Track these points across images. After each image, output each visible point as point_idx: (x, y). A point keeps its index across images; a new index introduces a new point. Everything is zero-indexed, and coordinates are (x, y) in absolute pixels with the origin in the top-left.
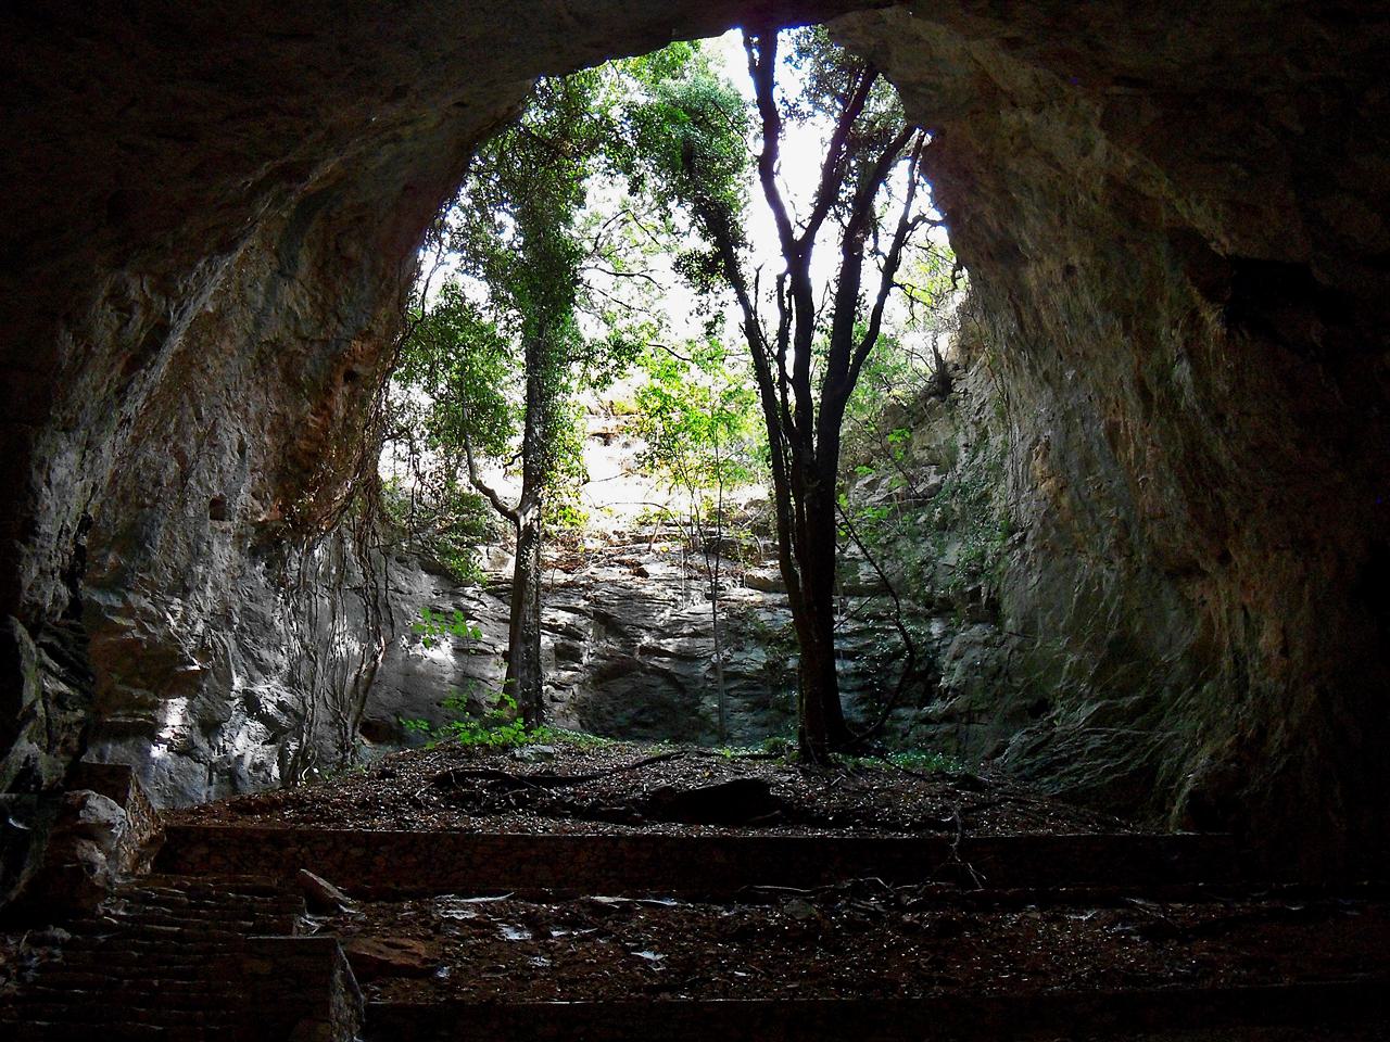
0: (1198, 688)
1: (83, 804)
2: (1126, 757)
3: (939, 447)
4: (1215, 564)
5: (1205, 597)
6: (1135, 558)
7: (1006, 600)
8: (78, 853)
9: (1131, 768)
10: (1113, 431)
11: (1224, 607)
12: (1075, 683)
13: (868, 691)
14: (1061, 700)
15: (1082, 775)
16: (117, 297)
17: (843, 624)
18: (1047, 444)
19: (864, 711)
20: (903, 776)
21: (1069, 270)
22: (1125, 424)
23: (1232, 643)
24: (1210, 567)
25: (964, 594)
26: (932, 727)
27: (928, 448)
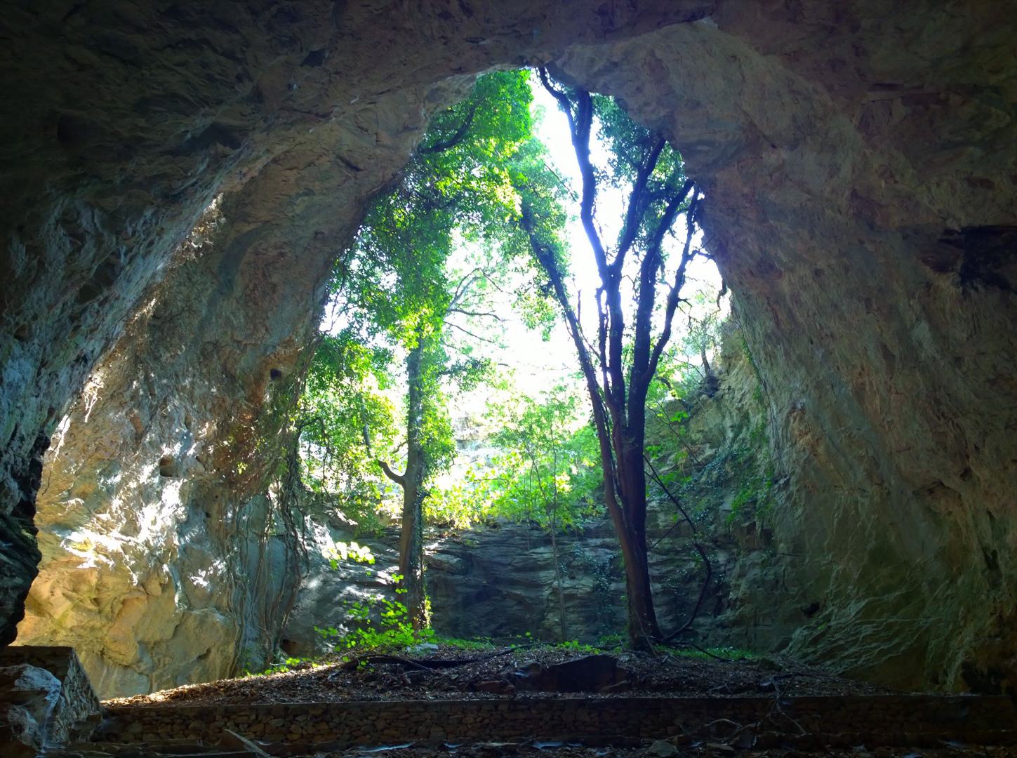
0: (953, 581)
1: (19, 675)
2: (896, 641)
3: (710, 430)
4: (957, 479)
5: (950, 509)
6: (886, 485)
7: (777, 530)
8: (9, 717)
9: (903, 648)
10: (859, 392)
11: (970, 515)
12: (843, 587)
13: (677, 603)
14: (832, 600)
15: (860, 656)
16: (68, 221)
17: (652, 558)
18: (803, 410)
19: (671, 620)
20: (719, 656)
21: (818, 273)
22: (871, 383)
23: (980, 542)
24: (954, 482)
25: (742, 529)
26: (726, 630)
27: (702, 431)
